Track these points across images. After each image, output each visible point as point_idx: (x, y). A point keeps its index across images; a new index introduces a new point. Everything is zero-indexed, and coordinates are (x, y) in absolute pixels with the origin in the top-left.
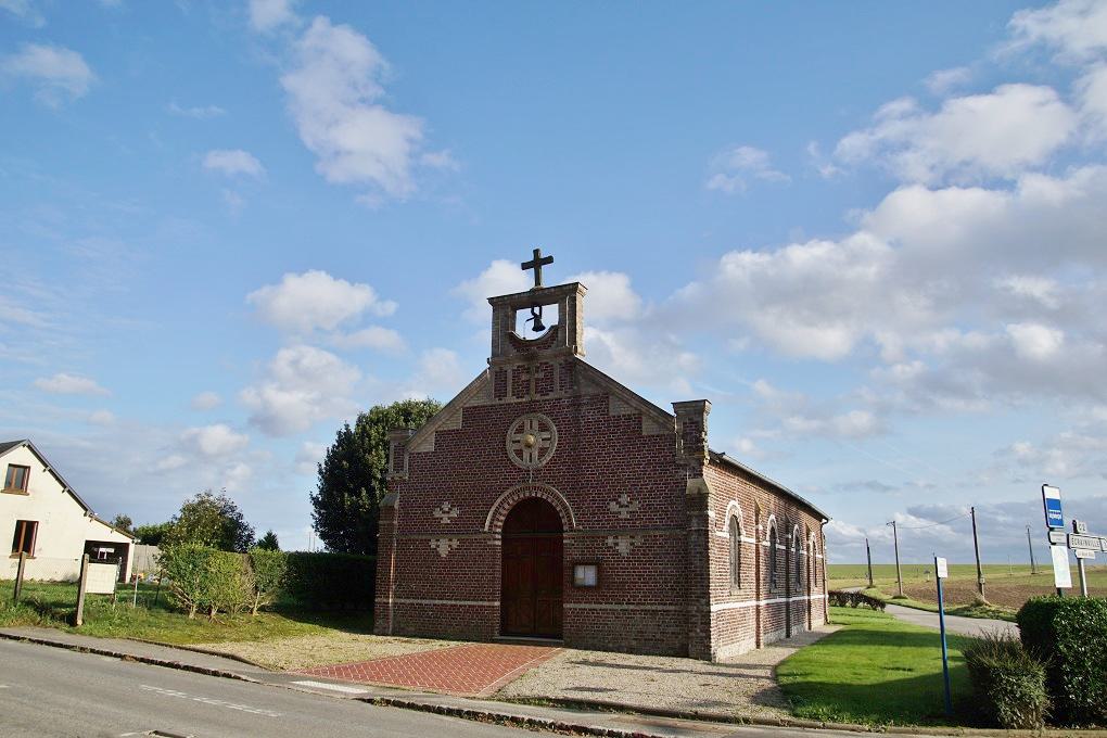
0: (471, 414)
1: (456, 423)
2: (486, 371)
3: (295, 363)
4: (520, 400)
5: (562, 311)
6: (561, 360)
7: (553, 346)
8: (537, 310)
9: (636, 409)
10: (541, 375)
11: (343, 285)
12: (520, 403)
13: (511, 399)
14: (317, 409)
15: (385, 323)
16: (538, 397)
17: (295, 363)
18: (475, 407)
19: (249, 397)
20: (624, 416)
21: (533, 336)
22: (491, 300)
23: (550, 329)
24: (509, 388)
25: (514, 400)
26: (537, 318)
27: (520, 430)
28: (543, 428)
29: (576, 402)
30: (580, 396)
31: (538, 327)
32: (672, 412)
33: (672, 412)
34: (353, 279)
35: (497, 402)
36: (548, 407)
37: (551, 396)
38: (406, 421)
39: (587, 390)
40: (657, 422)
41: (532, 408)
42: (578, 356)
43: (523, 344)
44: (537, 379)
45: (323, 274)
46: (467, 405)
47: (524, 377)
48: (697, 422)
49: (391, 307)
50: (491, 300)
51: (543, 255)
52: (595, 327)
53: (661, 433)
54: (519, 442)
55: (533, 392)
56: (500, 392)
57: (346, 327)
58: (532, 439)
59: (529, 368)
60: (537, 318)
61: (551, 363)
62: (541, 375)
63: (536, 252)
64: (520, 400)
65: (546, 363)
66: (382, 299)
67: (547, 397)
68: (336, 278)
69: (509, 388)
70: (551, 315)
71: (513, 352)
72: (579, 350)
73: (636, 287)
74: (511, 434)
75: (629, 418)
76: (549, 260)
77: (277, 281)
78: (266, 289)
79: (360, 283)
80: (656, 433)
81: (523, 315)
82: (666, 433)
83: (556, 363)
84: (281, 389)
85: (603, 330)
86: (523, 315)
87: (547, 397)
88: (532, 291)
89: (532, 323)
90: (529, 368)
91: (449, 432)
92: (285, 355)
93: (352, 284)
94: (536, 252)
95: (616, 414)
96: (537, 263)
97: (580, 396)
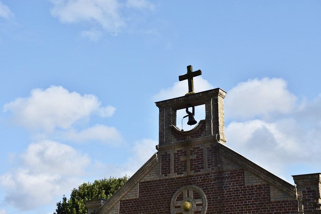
0: (146, 187)
1: (134, 194)
2: (155, 155)
3: (41, 154)
4: (180, 176)
5: (208, 110)
6: (208, 145)
7: (202, 135)
8: (190, 109)
9: (265, 181)
10: (194, 157)
11: (75, 96)
12: (180, 178)
13: (174, 175)
14: (58, 187)
15: (107, 122)
16: (192, 173)
17: (41, 154)
18: (148, 182)
19: (7, 181)
20: (256, 186)
21: (188, 128)
22: (158, 104)
23: (200, 123)
24: (172, 167)
25: (175, 176)
26: (191, 116)
27: (180, 198)
28: (197, 196)
29: (220, 176)
30: (223, 172)
31: (192, 122)
32: (292, 182)
33: (292, 182)
34: (82, 92)
35: (163, 177)
36: (199, 180)
37: (202, 172)
38: (107, 193)
39: (228, 167)
40: (281, 191)
41: (188, 181)
42: (221, 142)
43: (183, 134)
44: (191, 160)
45: (61, 88)
46: (143, 181)
47: (182, 159)
48: (314, 191)
49: (111, 110)
50: (158, 104)
51: (194, 70)
52: (261, 120)
53: (286, 199)
54: (179, 207)
55: (189, 170)
56: (166, 171)
57: (79, 126)
58: (188, 205)
59: (185, 152)
60: (191, 116)
61: (201, 148)
62: (194, 157)
63: (189, 68)
64: (180, 176)
65: (198, 148)
66: (104, 105)
67: (199, 173)
68: (70, 91)
69: (172, 167)
70: (200, 112)
71: (174, 141)
72: (221, 137)
73: (291, 88)
74: (174, 200)
75: (260, 187)
76: (198, 73)
77: (27, 94)
78: (18, 102)
79: (87, 94)
80: (281, 200)
81: (181, 113)
82: (289, 199)
83: (206, 147)
84: (31, 173)
85: (269, 121)
86: (181, 113)
87: (199, 173)
88: (187, 96)
89: (187, 119)
90: (185, 152)
91: (130, 201)
92: (34, 148)
93: (82, 95)
94: (189, 68)
95: (249, 185)
96: (190, 75)
97: (223, 172)
